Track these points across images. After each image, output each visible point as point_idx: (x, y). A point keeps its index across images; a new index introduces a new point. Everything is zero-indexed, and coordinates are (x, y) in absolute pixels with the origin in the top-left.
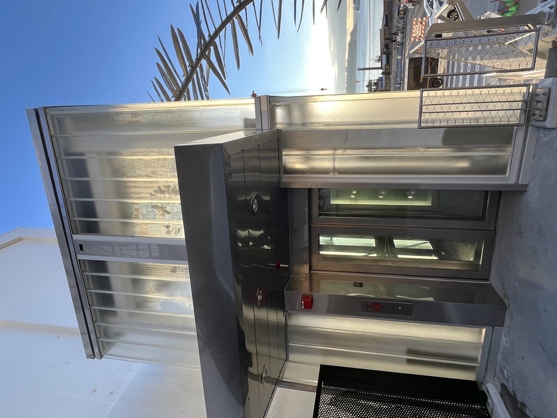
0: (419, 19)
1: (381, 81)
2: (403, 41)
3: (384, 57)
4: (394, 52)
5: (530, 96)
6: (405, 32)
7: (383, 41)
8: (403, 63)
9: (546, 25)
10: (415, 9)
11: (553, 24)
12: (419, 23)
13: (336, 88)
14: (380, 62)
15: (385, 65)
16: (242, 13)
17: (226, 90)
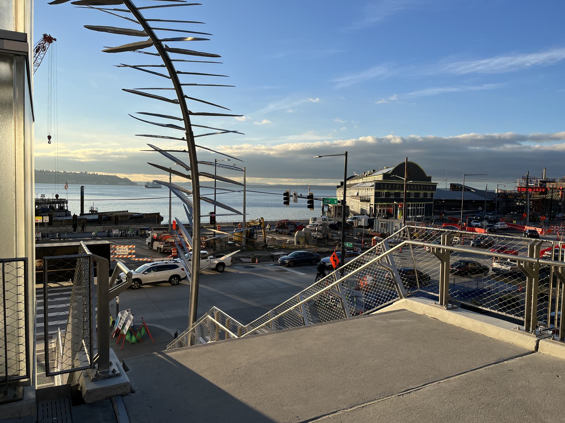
0: (134, 251)
1: (65, 215)
3: (96, 217)
4: (100, 228)
5: (15, 382)
6: (123, 238)
7: (114, 214)
8: (87, 238)
9: (97, 372)
10: (146, 245)
11: (96, 379)
12: (130, 251)
13: (57, 159)
14: (90, 213)
15: (86, 219)
16: (153, 49)
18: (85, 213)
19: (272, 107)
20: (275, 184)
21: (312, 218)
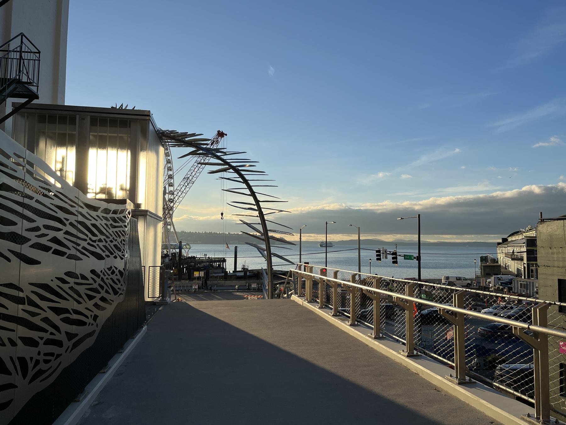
2: (252, 290)
4: (243, 282)
14: (242, 270)
17: (183, 156)
18: (238, 270)
19: (424, 158)
20: (436, 241)
21: (444, 277)
